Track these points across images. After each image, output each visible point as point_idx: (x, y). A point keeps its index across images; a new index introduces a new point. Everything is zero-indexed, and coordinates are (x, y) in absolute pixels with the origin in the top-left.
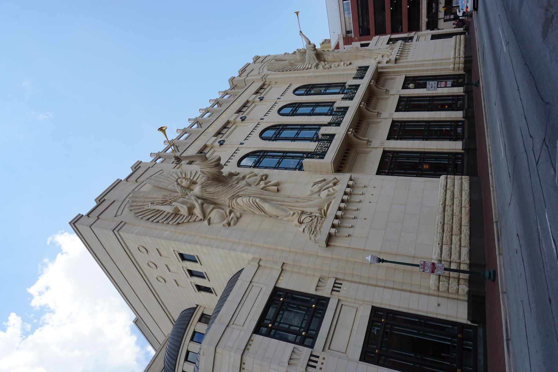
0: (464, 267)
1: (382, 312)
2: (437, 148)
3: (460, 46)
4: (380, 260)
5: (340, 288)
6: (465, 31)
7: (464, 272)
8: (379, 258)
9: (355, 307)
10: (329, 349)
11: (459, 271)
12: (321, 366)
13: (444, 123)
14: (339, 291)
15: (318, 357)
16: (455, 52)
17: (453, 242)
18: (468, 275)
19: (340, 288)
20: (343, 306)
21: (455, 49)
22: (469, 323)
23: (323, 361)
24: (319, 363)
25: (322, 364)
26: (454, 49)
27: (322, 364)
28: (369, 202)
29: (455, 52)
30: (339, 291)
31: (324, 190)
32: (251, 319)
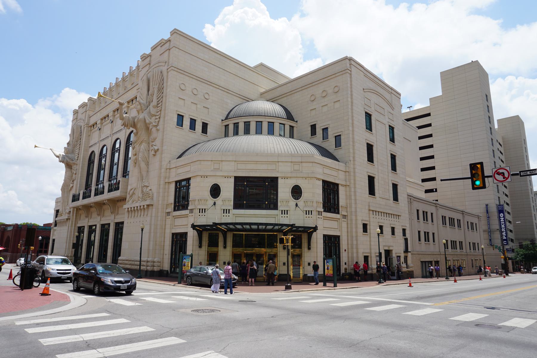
0: (142, 268)
1: (180, 237)
2: (372, 258)
3: (129, 265)
4: (142, 230)
5: (320, 215)
6: (341, 276)
7: (140, 267)
8: (143, 229)
9: (338, 227)
10: (236, 217)
11: (140, 265)
12: (227, 216)
13: (115, 253)
14: (318, 215)
15: (229, 213)
16: (123, 260)
17: (129, 261)
18: (425, 275)
19: (320, 215)
20: (337, 222)
21: (127, 260)
22: (341, 274)
23: (286, 217)
24: (309, 216)
25: (226, 216)
26: (127, 259)
27: (226, 216)
28: (536, 222)
29: (123, 260)
30: (318, 215)
31: (149, 159)
32: (364, 160)
